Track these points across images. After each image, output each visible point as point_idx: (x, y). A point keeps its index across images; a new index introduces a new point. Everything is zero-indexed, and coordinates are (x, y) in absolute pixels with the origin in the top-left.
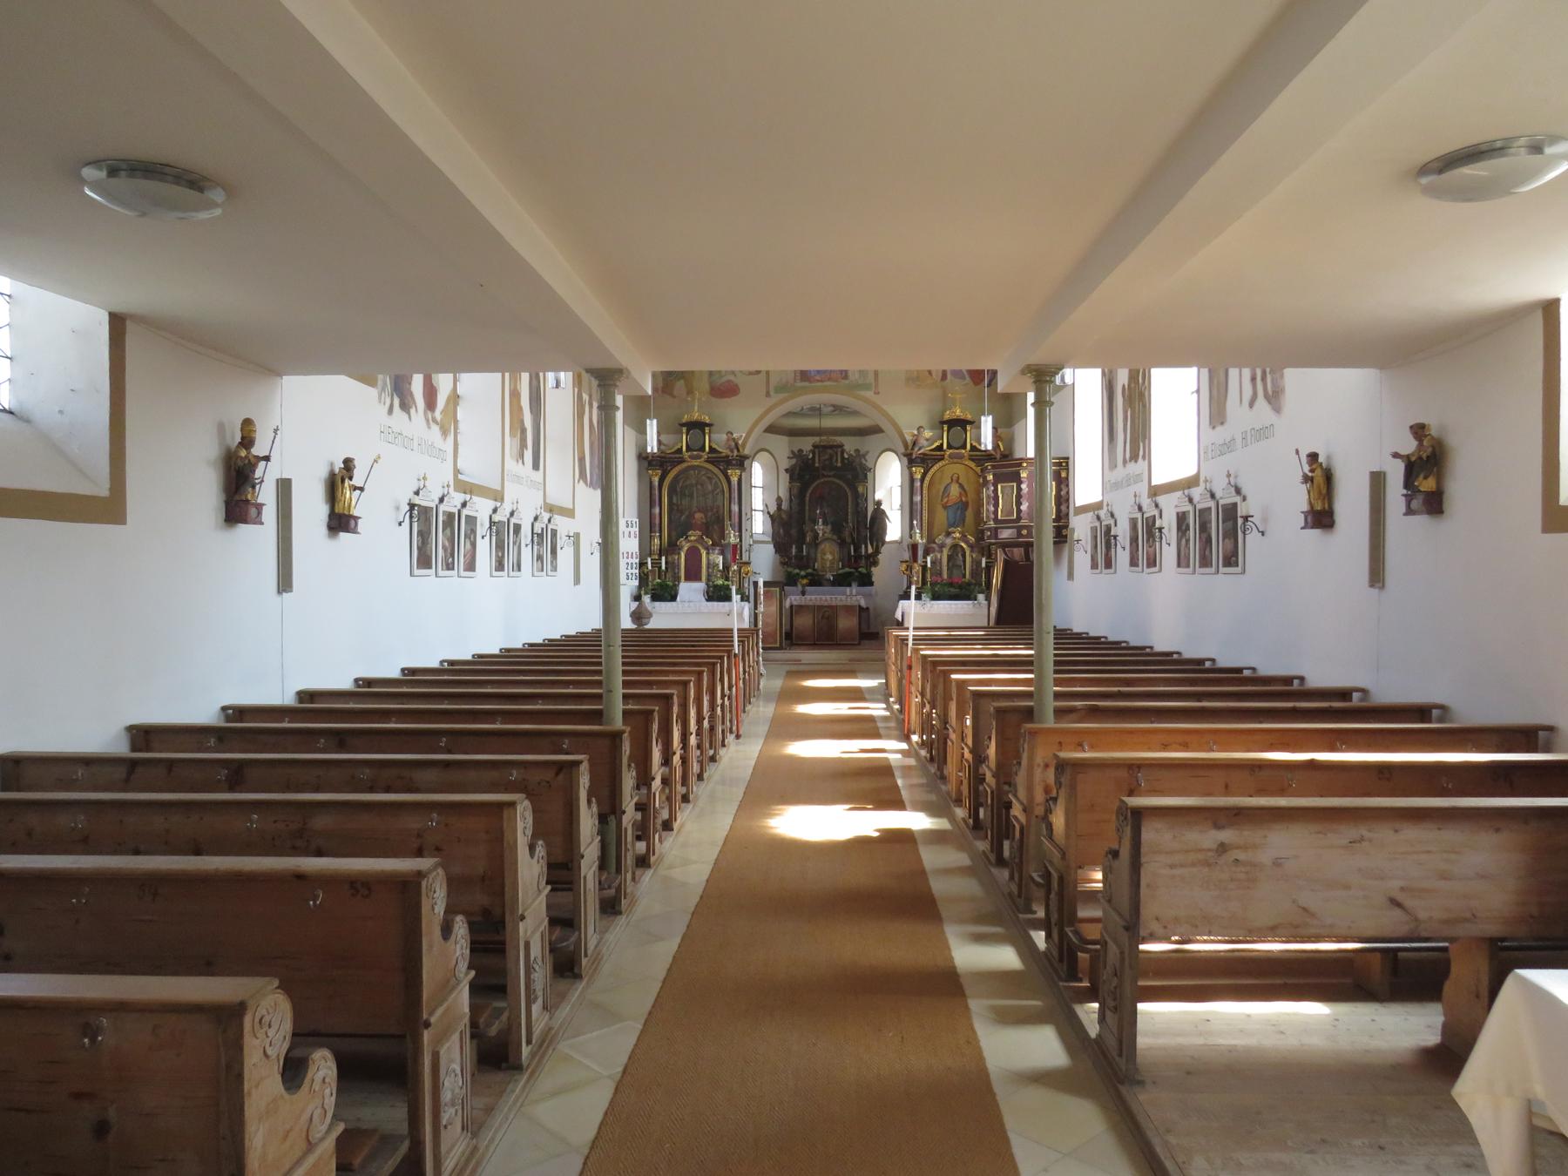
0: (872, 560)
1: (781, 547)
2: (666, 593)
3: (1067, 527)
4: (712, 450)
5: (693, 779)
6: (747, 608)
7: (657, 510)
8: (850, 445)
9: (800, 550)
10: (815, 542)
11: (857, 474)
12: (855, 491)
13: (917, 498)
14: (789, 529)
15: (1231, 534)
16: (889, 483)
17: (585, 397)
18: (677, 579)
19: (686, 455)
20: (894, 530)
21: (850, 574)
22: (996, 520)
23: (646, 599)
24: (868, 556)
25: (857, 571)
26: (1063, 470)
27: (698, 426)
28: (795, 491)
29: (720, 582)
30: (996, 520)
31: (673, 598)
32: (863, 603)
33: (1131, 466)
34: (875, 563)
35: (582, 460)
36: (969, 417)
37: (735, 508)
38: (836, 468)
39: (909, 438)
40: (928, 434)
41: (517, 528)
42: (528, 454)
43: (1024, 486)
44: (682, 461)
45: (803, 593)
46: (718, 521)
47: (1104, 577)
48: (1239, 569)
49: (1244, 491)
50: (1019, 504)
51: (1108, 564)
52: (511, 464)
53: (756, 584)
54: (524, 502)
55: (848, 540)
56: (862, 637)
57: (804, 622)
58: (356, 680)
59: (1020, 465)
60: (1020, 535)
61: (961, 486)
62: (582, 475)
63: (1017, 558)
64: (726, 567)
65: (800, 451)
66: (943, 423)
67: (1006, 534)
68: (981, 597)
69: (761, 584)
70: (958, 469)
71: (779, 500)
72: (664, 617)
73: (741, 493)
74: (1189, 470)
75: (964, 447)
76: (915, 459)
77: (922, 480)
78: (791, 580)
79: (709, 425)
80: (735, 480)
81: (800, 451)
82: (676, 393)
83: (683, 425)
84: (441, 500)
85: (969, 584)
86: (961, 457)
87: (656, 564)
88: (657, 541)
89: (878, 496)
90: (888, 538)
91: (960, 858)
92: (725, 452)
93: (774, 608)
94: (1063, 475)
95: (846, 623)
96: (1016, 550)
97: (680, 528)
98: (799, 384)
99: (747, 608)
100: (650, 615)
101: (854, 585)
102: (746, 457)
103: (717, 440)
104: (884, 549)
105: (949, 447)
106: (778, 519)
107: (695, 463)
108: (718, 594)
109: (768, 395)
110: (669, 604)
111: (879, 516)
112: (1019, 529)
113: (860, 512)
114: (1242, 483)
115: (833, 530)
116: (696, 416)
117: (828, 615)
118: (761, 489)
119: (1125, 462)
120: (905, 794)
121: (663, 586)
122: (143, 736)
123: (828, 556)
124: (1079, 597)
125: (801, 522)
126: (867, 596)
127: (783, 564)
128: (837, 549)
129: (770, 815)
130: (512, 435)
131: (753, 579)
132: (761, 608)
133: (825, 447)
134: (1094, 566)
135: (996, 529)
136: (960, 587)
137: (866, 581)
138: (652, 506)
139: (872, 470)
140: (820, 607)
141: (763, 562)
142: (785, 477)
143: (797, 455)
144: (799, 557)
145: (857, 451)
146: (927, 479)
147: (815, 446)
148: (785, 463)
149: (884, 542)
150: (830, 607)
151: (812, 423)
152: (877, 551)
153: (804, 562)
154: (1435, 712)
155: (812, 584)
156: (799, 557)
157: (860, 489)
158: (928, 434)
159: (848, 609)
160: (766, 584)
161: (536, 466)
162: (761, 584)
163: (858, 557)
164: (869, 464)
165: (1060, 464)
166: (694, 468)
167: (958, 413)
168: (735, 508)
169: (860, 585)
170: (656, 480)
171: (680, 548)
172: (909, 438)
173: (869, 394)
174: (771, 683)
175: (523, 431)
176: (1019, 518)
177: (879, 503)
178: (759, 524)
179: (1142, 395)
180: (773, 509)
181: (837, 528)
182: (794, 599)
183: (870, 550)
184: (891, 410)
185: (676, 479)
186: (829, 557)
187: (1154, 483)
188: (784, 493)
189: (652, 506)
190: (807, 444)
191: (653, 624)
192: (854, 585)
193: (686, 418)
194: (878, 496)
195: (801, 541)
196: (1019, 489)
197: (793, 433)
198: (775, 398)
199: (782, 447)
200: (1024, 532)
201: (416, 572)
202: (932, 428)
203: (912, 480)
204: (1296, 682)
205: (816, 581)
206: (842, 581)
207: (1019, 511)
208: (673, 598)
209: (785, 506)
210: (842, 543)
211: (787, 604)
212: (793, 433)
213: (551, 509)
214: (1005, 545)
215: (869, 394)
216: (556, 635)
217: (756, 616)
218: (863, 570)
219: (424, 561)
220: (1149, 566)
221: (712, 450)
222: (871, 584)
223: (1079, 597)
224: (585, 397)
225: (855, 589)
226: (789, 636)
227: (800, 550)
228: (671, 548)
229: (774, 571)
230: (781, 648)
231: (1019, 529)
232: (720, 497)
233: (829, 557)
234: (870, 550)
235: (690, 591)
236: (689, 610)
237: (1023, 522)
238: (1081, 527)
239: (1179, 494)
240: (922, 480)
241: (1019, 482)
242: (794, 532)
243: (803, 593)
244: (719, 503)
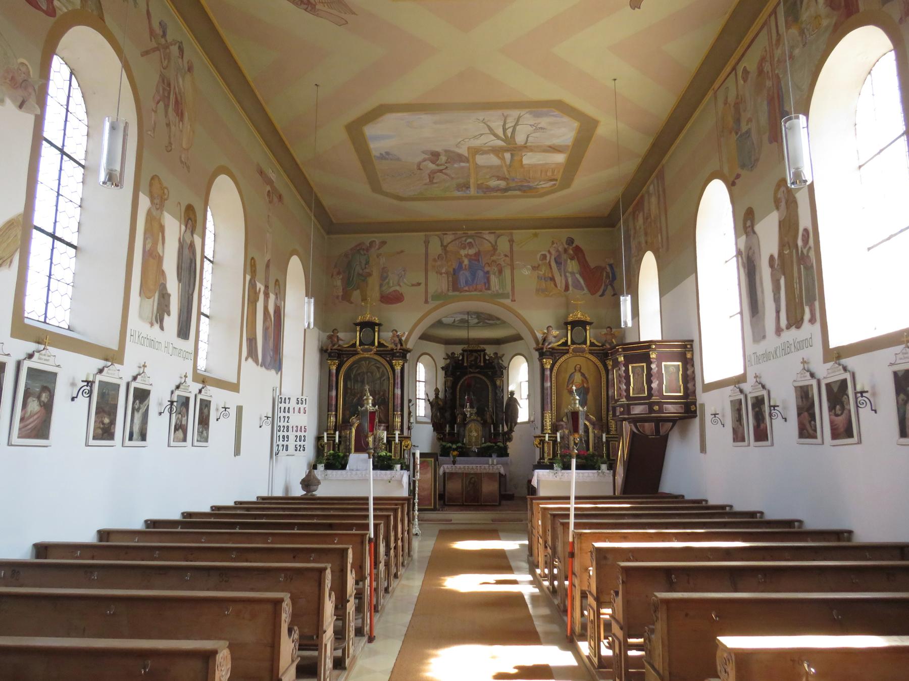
0: (508, 437)
1: (438, 426)
2: (337, 463)
3: (695, 403)
4: (380, 344)
5: (382, 593)
6: (405, 476)
7: (334, 393)
8: (490, 350)
9: (452, 428)
10: (464, 424)
11: (496, 371)
12: (495, 386)
13: (548, 384)
14: (444, 412)
15: (759, 417)
16: (519, 379)
17: (260, 286)
18: (349, 451)
19: (359, 348)
20: (523, 415)
21: (489, 448)
22: (628, 397)
23: (321, 467)
24: (504, 434)
25: (497, 441)
26: (687, 352)
27: (369, 326)
28: (449, 384)
29: (383, 453)
30: (628, 397)
31: (343, 467)
32: (502, 471)
33: (792, 335)
34: (510, 439)
35: (252, 341)
36: (588, 319)
37: (398, 392)
38: (481, 367)
39: (540, 336)
40: (555, 332)
41: (142, 395)
42: (172, 321)
43: (653, 366)
44: (356, 353)
45: (454, 463)
46: (391, 407)
47: (753, 450)
48: (769, 442)
49: (767, 387)
50: (649, 382)
51: (761, 435)
52: (136, 323)
53: (414, 454)
54: (157, 363)
55: (489, 421)
56: (506, 501)
57: (454, 487)
58: (183, 514)
59: (649, 347)
60: (651, 410)
61: (583, 375)
62: (252, 353)
63: (648, 432)
64: (389, 441)
65: (453, 354)
66: (566, 324)
67: (638, 410)
68: (604, 467)
69: (418, 455)
70: (579, 361)
71: (437, 391)
72: (332, 485)
73: (403, 380)
74: (737, 370)
75: (585, 342)
76: (545, 353)
77: (551, 370)
78: (445, 452)
79: (379, 325)
80: (398, 369)
81: (453, 354)
82: (352, 299)
83: (357, 324)
84: (135, 378)
85: (593, 456)
86: (583, 351)
87: (331, 438)
88: (333, 419)
89: (511, 388)
90: (519, 420)
91: (545, 611)
92: (390, 346)
93: (429, 475)
94: (689, 356)
95: (489, 488)
96: (646, 424)
97: (353, 406)
98: (451, 293)
99: (405, 476)
100: (319, 483)
101: (494, 456)
102: (408, 351)
103: (386, 337)
104: (516, 429)
105: (573, 343)
106: (435, 405)
107: (367, 355)
108: (382, 464)
109: (426, 302)
110: (340, 472)
111: (512, 404)
112: (651, 405)
113: (498, 400)
114: (764, 381)
115: (478, 414)
116: (368, 317)
117: (473, 481)
118: (423, 382)
119: (779, 331)
120: (540, 626)
121: (335, 456)
122: (42, 549)
123: (474, 433)
124: (710, 465)
125: (453, 407)
126: (505, 464)
127: (439, 439)
128: (480, 428)
129: (424, 671)
130: (144, 291)
131: (412, 451)
132: (418, 476)
133: (472, 351)
134: (738, 436)
135: (629, 405)
136: (586, 458)
137: (503, 452)
138: (330, 390)
139: (507, 368)
140: (467, 474)
141: (423, 438)
142: (441, 374)
143: (450, 356)
144: (451, 434)
145: (496, 354)
146: (555, 369)
147: (463, 350)
148: (442, 363)
149: (516, 423)
150: (476, 474)
151: (461, 334)
152: (511, 430)
153: (455, 438)
154: (796, 524)
155: (460, 455)
156: (451, 434)
157: (498, 383)
158: (555, 332)
159: (491, 476)
160: (422, 455)
161: (183, 332)
162: (418, 455)
163: (497, 434)
164: (505, 364)
165: (685, 346)
166: (365, 359)
167: (579, 316)
168: (398, 392)
169: (498, 456)
170: (334, 368)
171: (352, 425)
172: (540, 336)
173: (507, 302)
174: (422, 546)
175: (164, 297)
176: (650, 395)
177: (512, 393)
178: (422, 409)
179: (803, 259)
180: (432, 397)
181: (481, 412)
182: (446, 467)
183: (506, 429)
184: (524, 313)
185: (350, 368)
186: (474, 434)
187: (833, 344)
188: (441, 387)
189: (330, 390)
190: (458, 350)
191: (321, 491)
192: (494, 456)
193: (360, 319)
194: (511, 388)
195: (453, 422)
196: (649, 369)
197: (447, 342)
198: (433, 304)
199: (439, 352)
200: (656, 408)
201: (196, 443)
202: (558, 328)
203: (543, 370)
204: (728, 508)
205: (464, 452)
206: (484, 453)
207: (650, 389)
208: (343, 467)
209: (441, 395)
210: (484, 424)
211: (441, 472)
212: (447, 342)
213: (204, 380)
214: (635, 420)
215: (507, 302)
216: (171, 511)
217: (414, 482)
218: (501, 444)
219: (105, 432)
220: (835, 435)
221: (380, 344)
222: (507, 455)
223: (710, 465)
224: (260, 286)
225: (494, 459)
226: (442, 497)
227: (452, 428)
228: (345, 425)
229: (433, 445)
230: (434, 509)
231: (651, 405)
232: (386, 382)
233: (474, 434)
234: (506, 429)
235: (359, 462)
236: (360, 480)
237: (654, 399)
238: (714, 404)
239: (732, 387)
240: (551, 370)
241: (649, 362)
242: (447, 415)
243: (454, 463)
244: (385, 387)
